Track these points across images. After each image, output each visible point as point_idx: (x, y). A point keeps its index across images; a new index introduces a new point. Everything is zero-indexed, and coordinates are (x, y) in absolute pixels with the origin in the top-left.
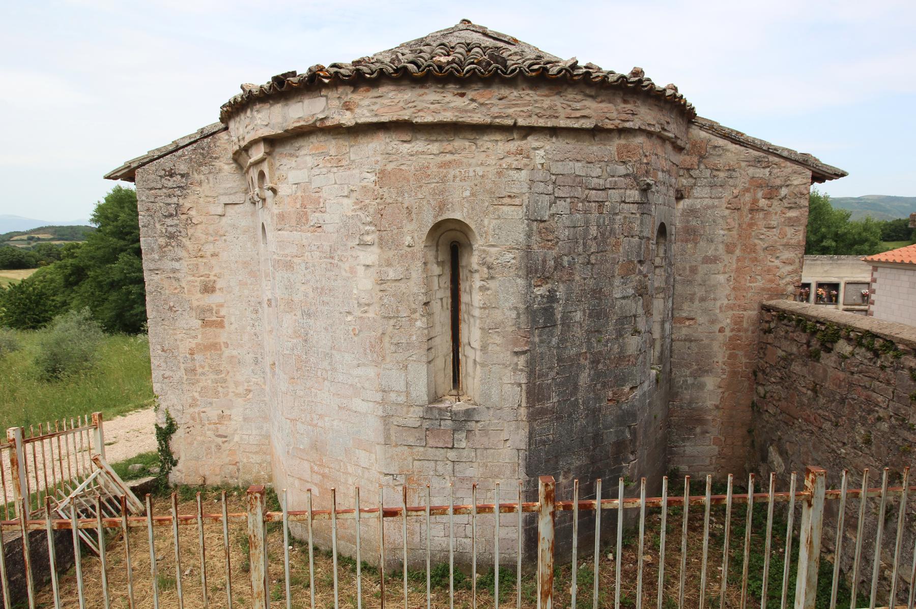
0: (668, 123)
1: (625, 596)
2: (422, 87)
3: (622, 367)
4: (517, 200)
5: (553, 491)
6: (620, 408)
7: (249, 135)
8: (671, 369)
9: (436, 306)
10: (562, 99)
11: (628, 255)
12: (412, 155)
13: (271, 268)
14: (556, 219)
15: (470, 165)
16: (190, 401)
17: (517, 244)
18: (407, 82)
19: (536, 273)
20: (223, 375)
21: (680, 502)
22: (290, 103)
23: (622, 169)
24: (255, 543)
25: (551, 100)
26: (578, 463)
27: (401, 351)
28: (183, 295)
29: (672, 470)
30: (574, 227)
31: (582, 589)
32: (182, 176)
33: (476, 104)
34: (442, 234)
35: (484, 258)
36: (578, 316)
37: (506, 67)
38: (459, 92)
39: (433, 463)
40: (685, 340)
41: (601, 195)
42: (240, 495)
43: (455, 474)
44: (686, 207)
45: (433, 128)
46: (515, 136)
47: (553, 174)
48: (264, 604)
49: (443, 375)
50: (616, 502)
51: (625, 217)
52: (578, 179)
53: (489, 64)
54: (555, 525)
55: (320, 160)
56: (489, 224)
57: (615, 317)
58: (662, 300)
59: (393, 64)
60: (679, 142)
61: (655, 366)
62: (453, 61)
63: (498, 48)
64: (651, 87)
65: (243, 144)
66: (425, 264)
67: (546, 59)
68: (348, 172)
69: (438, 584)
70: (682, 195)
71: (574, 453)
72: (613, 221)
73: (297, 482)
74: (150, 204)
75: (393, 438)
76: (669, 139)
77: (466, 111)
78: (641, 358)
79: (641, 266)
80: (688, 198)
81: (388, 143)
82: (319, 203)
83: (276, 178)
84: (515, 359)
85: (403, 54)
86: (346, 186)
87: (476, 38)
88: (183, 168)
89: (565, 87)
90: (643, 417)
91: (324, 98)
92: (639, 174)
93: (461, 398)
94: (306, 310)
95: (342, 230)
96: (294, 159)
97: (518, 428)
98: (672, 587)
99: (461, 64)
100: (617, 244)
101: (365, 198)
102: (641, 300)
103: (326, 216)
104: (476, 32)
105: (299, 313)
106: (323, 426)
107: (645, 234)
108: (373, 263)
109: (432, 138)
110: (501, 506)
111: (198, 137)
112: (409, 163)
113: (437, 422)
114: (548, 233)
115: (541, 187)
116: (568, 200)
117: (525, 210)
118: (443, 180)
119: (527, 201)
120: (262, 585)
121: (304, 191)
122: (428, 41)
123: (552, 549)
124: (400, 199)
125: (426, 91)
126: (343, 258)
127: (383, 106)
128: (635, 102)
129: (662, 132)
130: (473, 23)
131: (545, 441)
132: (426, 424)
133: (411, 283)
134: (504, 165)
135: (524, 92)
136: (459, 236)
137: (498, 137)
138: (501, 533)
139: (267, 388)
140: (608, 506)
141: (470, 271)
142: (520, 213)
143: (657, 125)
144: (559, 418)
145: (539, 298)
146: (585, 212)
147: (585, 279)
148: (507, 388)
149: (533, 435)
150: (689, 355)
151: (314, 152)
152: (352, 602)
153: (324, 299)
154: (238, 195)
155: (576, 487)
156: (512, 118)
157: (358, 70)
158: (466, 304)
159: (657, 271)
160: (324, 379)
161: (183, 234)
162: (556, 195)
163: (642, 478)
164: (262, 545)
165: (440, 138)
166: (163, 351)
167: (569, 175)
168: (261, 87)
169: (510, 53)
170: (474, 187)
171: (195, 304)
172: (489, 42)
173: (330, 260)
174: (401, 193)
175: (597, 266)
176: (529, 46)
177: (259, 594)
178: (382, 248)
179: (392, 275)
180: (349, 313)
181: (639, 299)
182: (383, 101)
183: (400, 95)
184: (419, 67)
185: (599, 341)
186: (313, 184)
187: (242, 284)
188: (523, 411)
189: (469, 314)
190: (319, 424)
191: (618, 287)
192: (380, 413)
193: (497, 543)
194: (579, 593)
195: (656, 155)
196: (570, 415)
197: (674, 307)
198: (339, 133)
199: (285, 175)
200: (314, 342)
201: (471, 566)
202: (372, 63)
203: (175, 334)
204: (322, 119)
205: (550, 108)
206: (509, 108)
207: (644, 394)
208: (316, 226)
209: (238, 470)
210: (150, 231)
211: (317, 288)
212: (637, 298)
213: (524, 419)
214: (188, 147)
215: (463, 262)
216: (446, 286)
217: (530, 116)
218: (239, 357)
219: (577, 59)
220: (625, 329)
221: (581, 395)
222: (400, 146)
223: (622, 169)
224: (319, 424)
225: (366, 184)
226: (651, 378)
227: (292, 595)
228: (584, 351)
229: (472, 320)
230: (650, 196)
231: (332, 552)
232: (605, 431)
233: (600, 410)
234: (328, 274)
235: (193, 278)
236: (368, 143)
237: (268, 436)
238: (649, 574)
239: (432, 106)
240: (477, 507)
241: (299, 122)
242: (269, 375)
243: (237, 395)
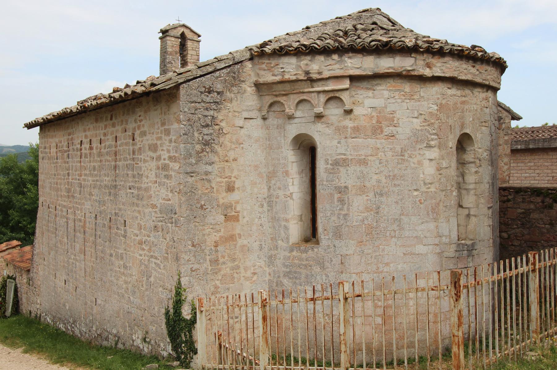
16: (213, 289)
28: (212, 194)
32: (218, 93)
68: (418, 103)
74: (190, 115)
82: (393, 121)
86: (416, 112)
88: (219, 87)
91: (414, 59)
96: (371, 92)
101: (431, 119)
103: (399, 129)
108: (435, 157)
111: (231, 64)
113: (461, 252)
118: (463, 112)
126: (412, 156)
127: (447, 68)
151: (391, 88)
153: (396, 182)
161: (216, 142)
166: (193, 246)
171: (221, 201)
173: (402, 157)
174: (448, 117)
178: (440, 149)
203: (204, 230)
210: (189, 139)
211: (390, 176)
214: (224, 70)
218: (249, 245)
225: (432, 111)
235: (220, 179)
236: (433, 87)
241: (389, 69)
243: (246, 279)
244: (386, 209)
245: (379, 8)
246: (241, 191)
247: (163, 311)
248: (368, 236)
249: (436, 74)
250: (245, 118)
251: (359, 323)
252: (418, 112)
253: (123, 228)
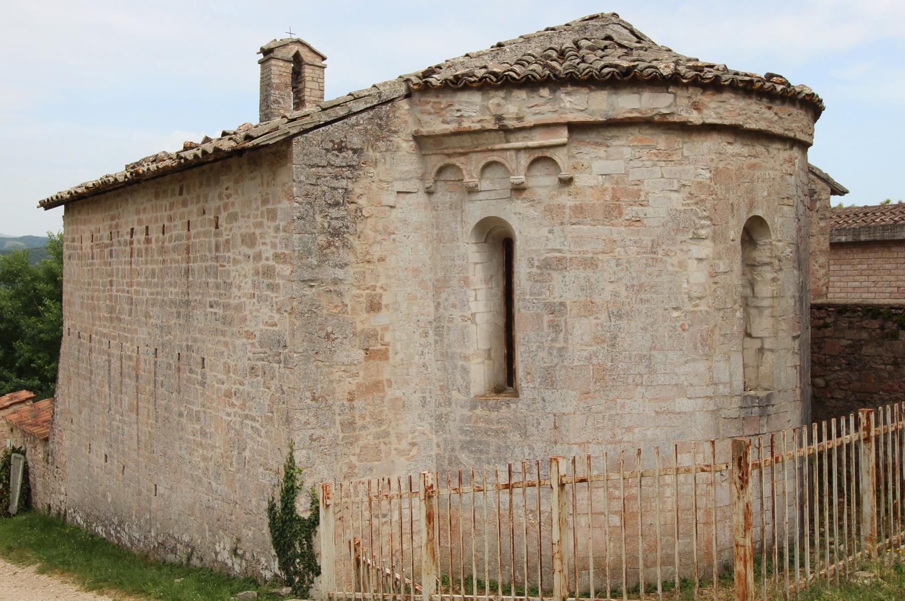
16: (345, 469)
28: (345, 315)
32: (355, 151)
68: (679, 168)
74: (309, 187)
86: (675, 181)
88: (356, 141)
91: (672, 96)
96: (603, 149)
101: (701, 193)
103: (648, 210)
108: (707, 256)
111: (375, 103)
113: (749, 410)
118: (752, 182)
124: (727, 196)
126: (669, 253)
127: (726, 110)
151: (635, 144)
161: (351, 230)
166: (314, 399)
171: (360, 327)
173: (652, 256)
174: (728, 191)
178: (714, 241)
179: (722, 268)
183: (736, 102)
203: (331, 373)
210: (307, 225)
211: (633, 286)
214: (363, 114)
218: (404, 398)
225: (702, 180)
234: (649, 270)
235: (358, 291)
236: (703, 142)
241: (632, 113)
243: (400, 453)
244: (628, 339)
245: (616, 12)
246: (391, 310)
247: (265, 505)
249: (709, 121)
250: (398, 192)
251: (583, 525)
252: (679, 181)
253: (199, 371)
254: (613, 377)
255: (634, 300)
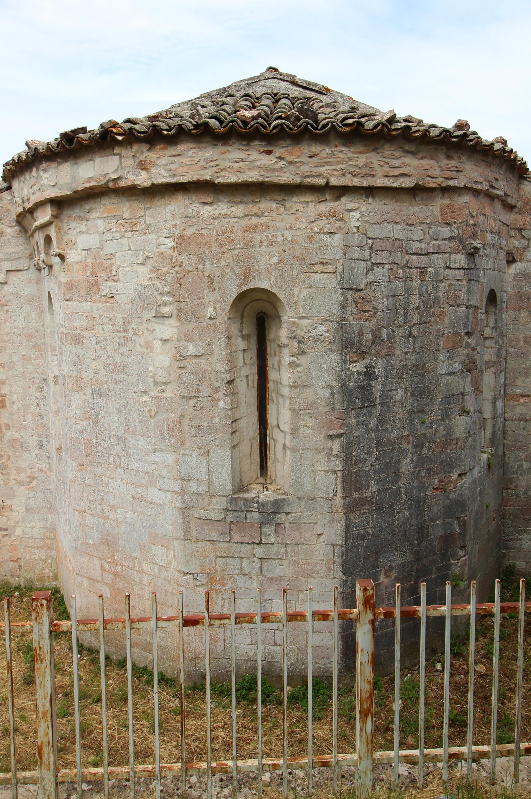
0: (497, 180)
1: (455, 712)
2: (224, 144)
3: (449, 451)
4: (330, 266)
5: (372, 596)
6: (448, 498)
7: (35, 196)
8: (504, 453)
9: (241, 385)
10: (378, 156)
11: (454, 327)
12: (214, 219)
13: (58, 342)
14: (374, 287)
15: (278, 229)
17: (330, 316)
18: (207, 139)
19: (352, 348)
20: (4, 461)
21: (515, 608)
22: (80, 161)
23: (446, 232)
24: (40, 656)
25: (367, 158)
26: (401, 560)
27: (202, 434)
29: (507, 567)
30: (394, 296)
31: (407, 704)
33: (284, 163)
34: (248, 304)
35: (294, 331)
36: (399, 395)
37: (316, 121)
38: (266, 149)
39: (238, 561)
40: (520, 420)
41: (423, 261)
42: (21, 596)
43: (263, 573)
44: (518, 271)
45: (237, 189)
46: (328, 197)
47: (370, 238)
48: (50, 725)
49: (249, 461)
50: (443, 608)
51: (450, 285)
52: (397, 244)
53: (298, 119)
54: (374, 630)
55: (112, 224)
56: (299, 293)
57: (441, 396)
58: (493, 375)
59: (193, 119)
60: (509, 200)
61: (486, 450)
62: (259, 116)
63: (308, 99)
64: (478, 141)
65: (28, 206)
66: (229, 338)
67: (361, 111)
68: (144, 237)
69: (244, 698)
70: (514, 258)
71: (396, 548)
72: (436, 289)
73: (85, 582)
75: (194, 532)
76: (498, 197)
77: (273, 170)
78: (470, 441)
79: (469, 338)
80: (520, 261)
81: (187, 206)
82: (112, 270)
83: (64, 243)
84: (329, 443)
85: (203, 107)
86: (141, 253)
87: (284, 87)
89: (382, 142)
90: (473, 507)
91: (118, 157)
92: (465, 236)
93: (269, 487)
94: (97, 389)
95: (137, 301)
96: (84, 223)
97: (333, 521)
98: (509, 702)
99: (267, 118)
100: (442, 314)
101: (163, 265)
102: (470, 377)
103: (120, 286)
104: (284, 80)
105: (89, 392)
106: (115, 518)
107: (473, 303)
109: (236, 200)
110: (314, 614)
112: (211, 227)
113: (242, 515)
114: (365, 304)
115: (356, 253)
116: (387, 266)
117: (339, 278)
118: (249, 245)
119: (341, 267)
120: (48, 704)
121: (95, 258)
122: (231, 91)
123: (372, 662)
125: (229, 148)
126: (137, 332)
128: (460, 158)
129: (491, 190)
130: (281, 70)
131: (363, 536)
132: (231, 517)
133: (213, 359)
134: (316, 229)
135: (337, 149)
136: (266, 307)
137: (308, 198)
138: (314, 640)
139: (53, 475)
140: (434, 613)
141: (279, 346)
142: (333, 281)
143: (484, 183)
144: (380, 509)
145: (356, 376)
146: (406, 279)
147: (406, 353)
148: (321, 476)
149: (350, 529)
150: (524, 436)
152: (147, 720)
153: (117, 376)
154: (22, 261)
155: (398, 592)
156: (324, 178)
157: (154, 126)
158: (274, 381)
159: (487, 342)
160: (117, 466)
162: (373, 261)
163: (472, 582)
164: (49, 658)
165: (245, 200)
167: (387, 239)
168: (48, 144)
169: (321, 104)
170: (282, 252)
172: (297, 92)
174: (202, 260)
175: (419, 339)
176: (342, 96)
177: (44, 714)
178: (180, 320)
179: (192, 350)
180: (144, 392)
181: (467, 375)
182: (182, 160)
183: (200, 153)
184: (221, 122)
185: (422, 423)
186: (105, 250)
187: (26, 359)
188: (339, 502)
189: (278, 393)
190: (111, 517)
191: (443, 362)
192: (179, 504)
193: (310, 650)
194: (404, 709)
195: (484, 215)
196: (391, 506)
197: (507, 382)
198: (133, 195)
199: (73, 240)
200: (106, 424)
201: (281, 677)
202: (170, 118)
204: (115, 180)
205: (366, 166)
206: (321, 166)
207: (474, 482)
208: (108, 295)
209: (20, 567)
211: (109, 365)
212: (464, 374)
213: (340, 511)
215: (271, 335)
216: (252, 361)
217: (344, 175)
218: (22, 440)
219: (396, 112)
220: (451, 408)
221: (403, 483)
222: (201, 208)
223: (446, 232)
224: (111, 517)
226: (482, 463)
227: (80, 711)
228: (406, 433)
229: (281, 400)
230: (478, 260)
231: (125, 661)
232: (432, 524)
233: (424, 500)
234: (121, 349)
236: (166, 205)
237: (53, 529)
238: (482, 687)
239: (236, 165)
240: (288, 615)
241: (90, 182)
242: (55, 460)
243: (20, 483)
244: (107, 419)
245: (273, 66)
246: (7, 369)
248: (89, 458)
249: (159, 181)
250: (8, 271)
251: (85, 586)
252: (144, 254)
254: (98, 454)
255: (110, 379)
